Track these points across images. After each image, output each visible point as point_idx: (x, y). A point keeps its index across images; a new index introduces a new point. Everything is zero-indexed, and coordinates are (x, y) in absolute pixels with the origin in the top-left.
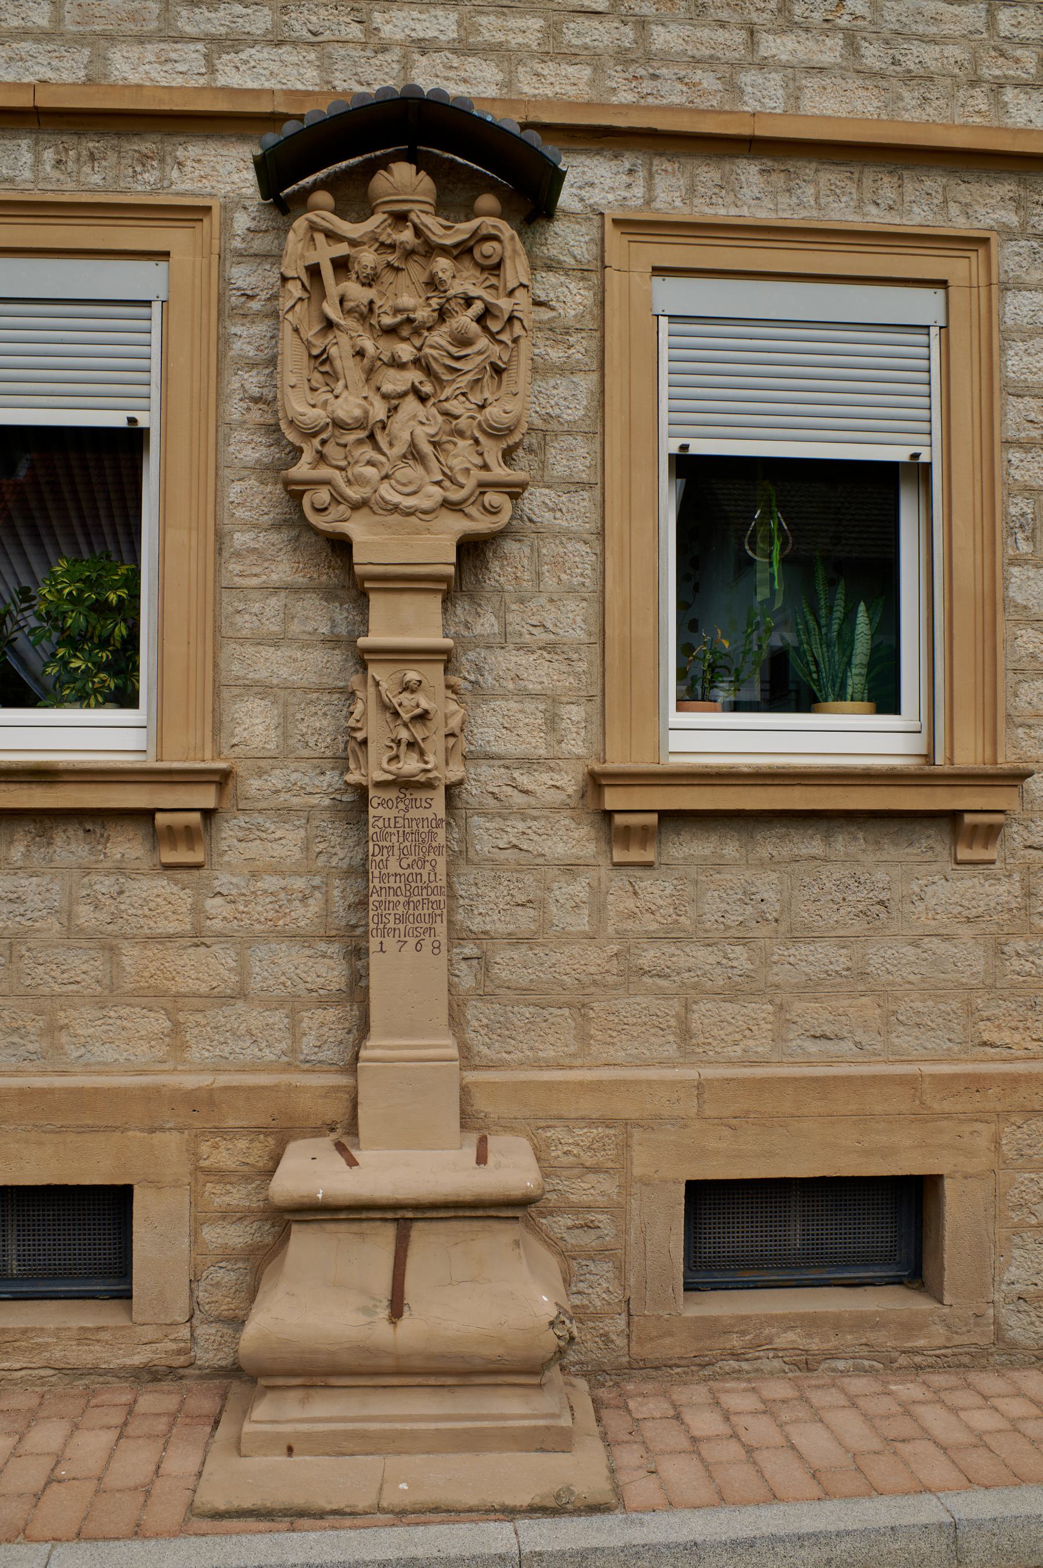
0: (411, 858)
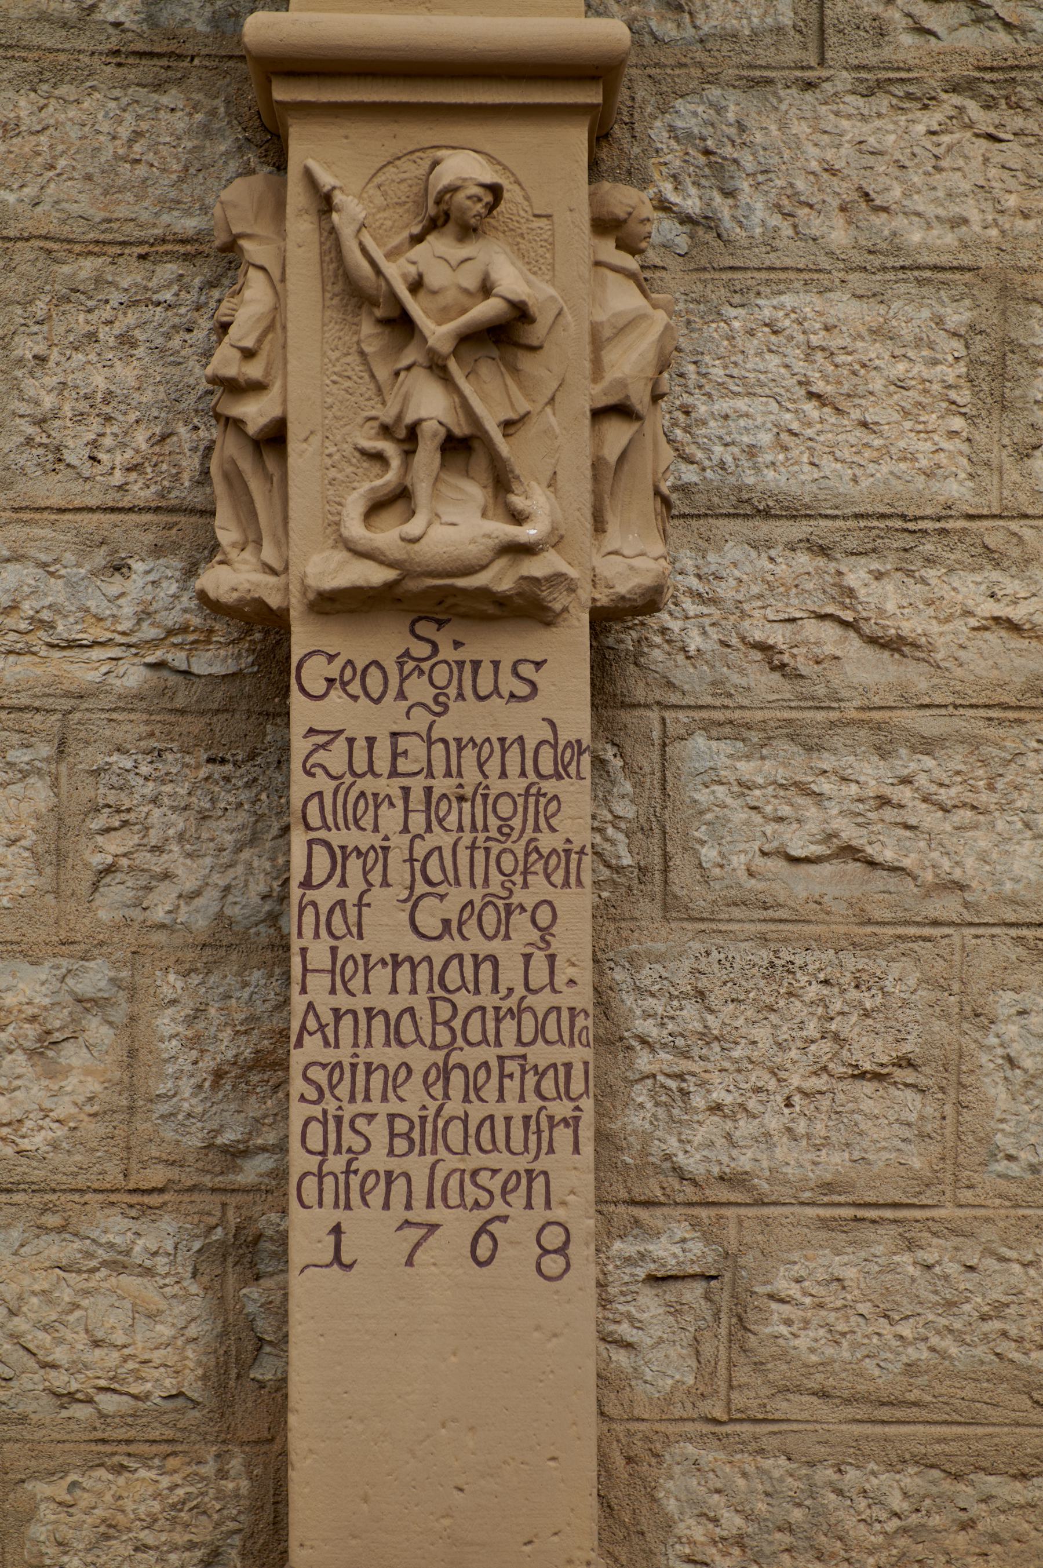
0: (458, 896)
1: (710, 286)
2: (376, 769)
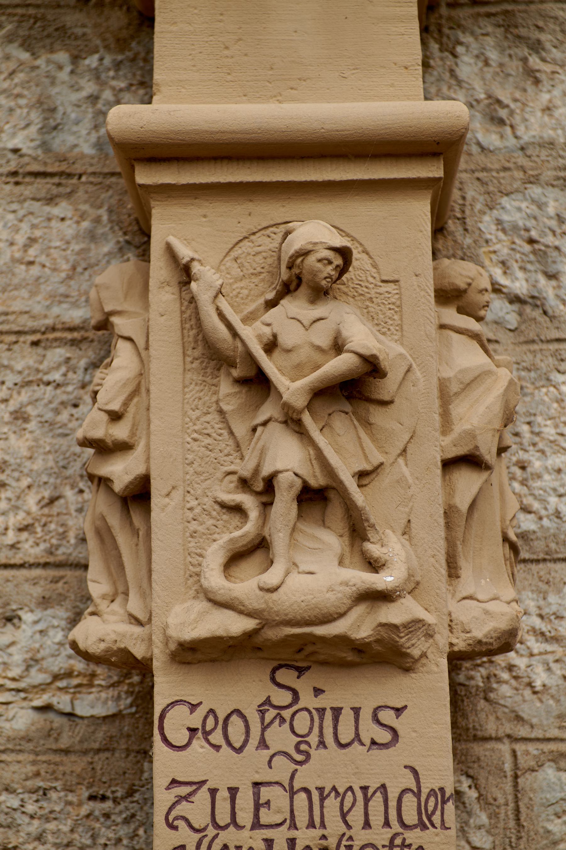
1: (539, 356)
2: (239, 820)
